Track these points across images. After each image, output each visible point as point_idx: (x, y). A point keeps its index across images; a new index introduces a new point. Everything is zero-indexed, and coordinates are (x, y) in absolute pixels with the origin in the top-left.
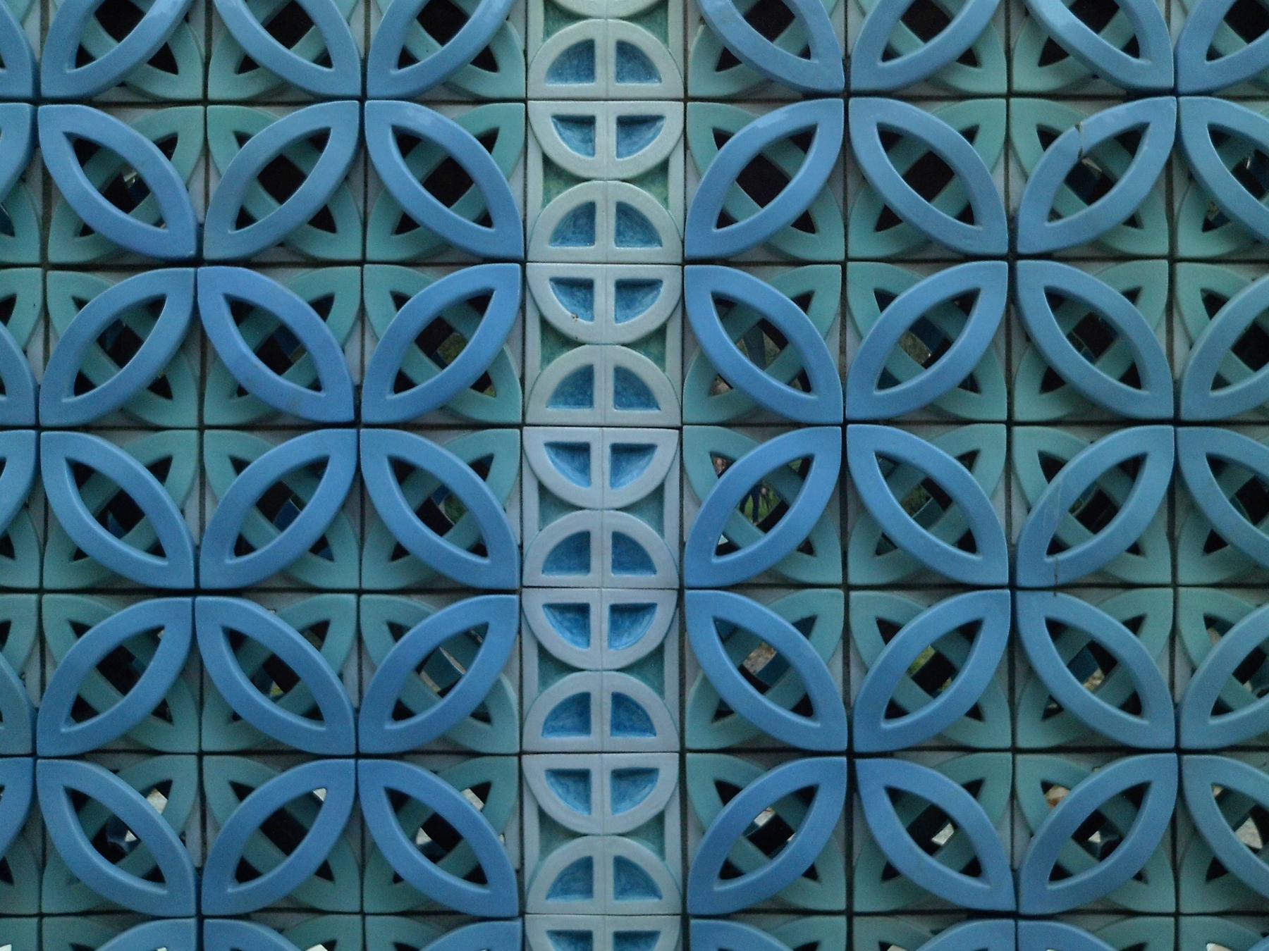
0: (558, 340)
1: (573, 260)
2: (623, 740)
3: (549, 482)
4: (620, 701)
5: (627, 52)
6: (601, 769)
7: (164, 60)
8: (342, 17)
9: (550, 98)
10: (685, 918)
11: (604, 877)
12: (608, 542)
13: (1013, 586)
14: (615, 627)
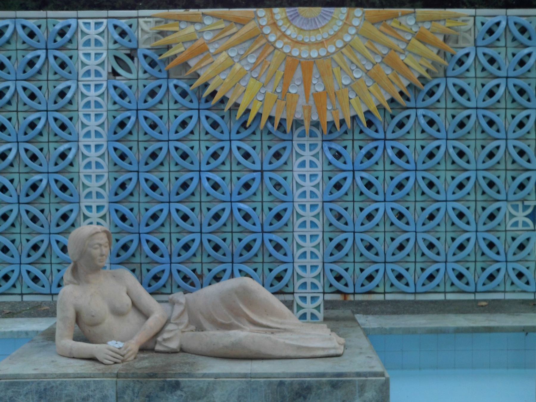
0: (299, 216)
1: (303, 262)
2: (313, 229)
3: (299, 303)
4: (311, 192)
5: (311, 162)
6: (309, 296)
7: (41, 134)
8: (227, 247)
9: (297, 171)
10: (324, 263)
11: (308, 255)
12: (310, 315)
13: (354, 262)
14: (311, 269)
